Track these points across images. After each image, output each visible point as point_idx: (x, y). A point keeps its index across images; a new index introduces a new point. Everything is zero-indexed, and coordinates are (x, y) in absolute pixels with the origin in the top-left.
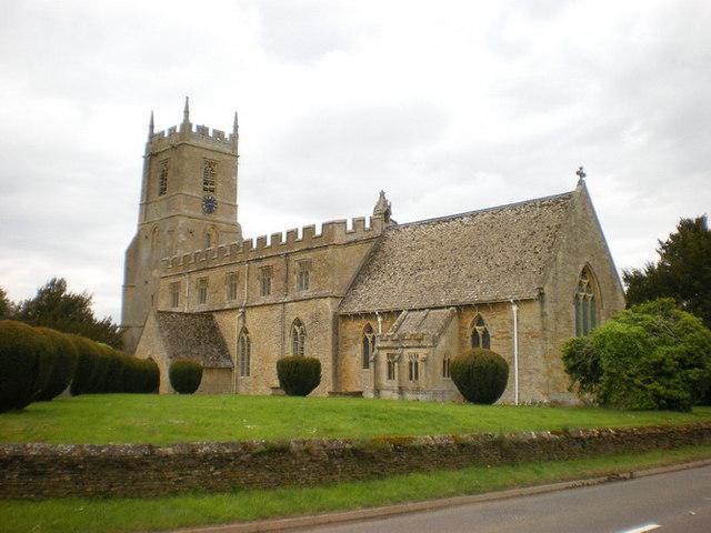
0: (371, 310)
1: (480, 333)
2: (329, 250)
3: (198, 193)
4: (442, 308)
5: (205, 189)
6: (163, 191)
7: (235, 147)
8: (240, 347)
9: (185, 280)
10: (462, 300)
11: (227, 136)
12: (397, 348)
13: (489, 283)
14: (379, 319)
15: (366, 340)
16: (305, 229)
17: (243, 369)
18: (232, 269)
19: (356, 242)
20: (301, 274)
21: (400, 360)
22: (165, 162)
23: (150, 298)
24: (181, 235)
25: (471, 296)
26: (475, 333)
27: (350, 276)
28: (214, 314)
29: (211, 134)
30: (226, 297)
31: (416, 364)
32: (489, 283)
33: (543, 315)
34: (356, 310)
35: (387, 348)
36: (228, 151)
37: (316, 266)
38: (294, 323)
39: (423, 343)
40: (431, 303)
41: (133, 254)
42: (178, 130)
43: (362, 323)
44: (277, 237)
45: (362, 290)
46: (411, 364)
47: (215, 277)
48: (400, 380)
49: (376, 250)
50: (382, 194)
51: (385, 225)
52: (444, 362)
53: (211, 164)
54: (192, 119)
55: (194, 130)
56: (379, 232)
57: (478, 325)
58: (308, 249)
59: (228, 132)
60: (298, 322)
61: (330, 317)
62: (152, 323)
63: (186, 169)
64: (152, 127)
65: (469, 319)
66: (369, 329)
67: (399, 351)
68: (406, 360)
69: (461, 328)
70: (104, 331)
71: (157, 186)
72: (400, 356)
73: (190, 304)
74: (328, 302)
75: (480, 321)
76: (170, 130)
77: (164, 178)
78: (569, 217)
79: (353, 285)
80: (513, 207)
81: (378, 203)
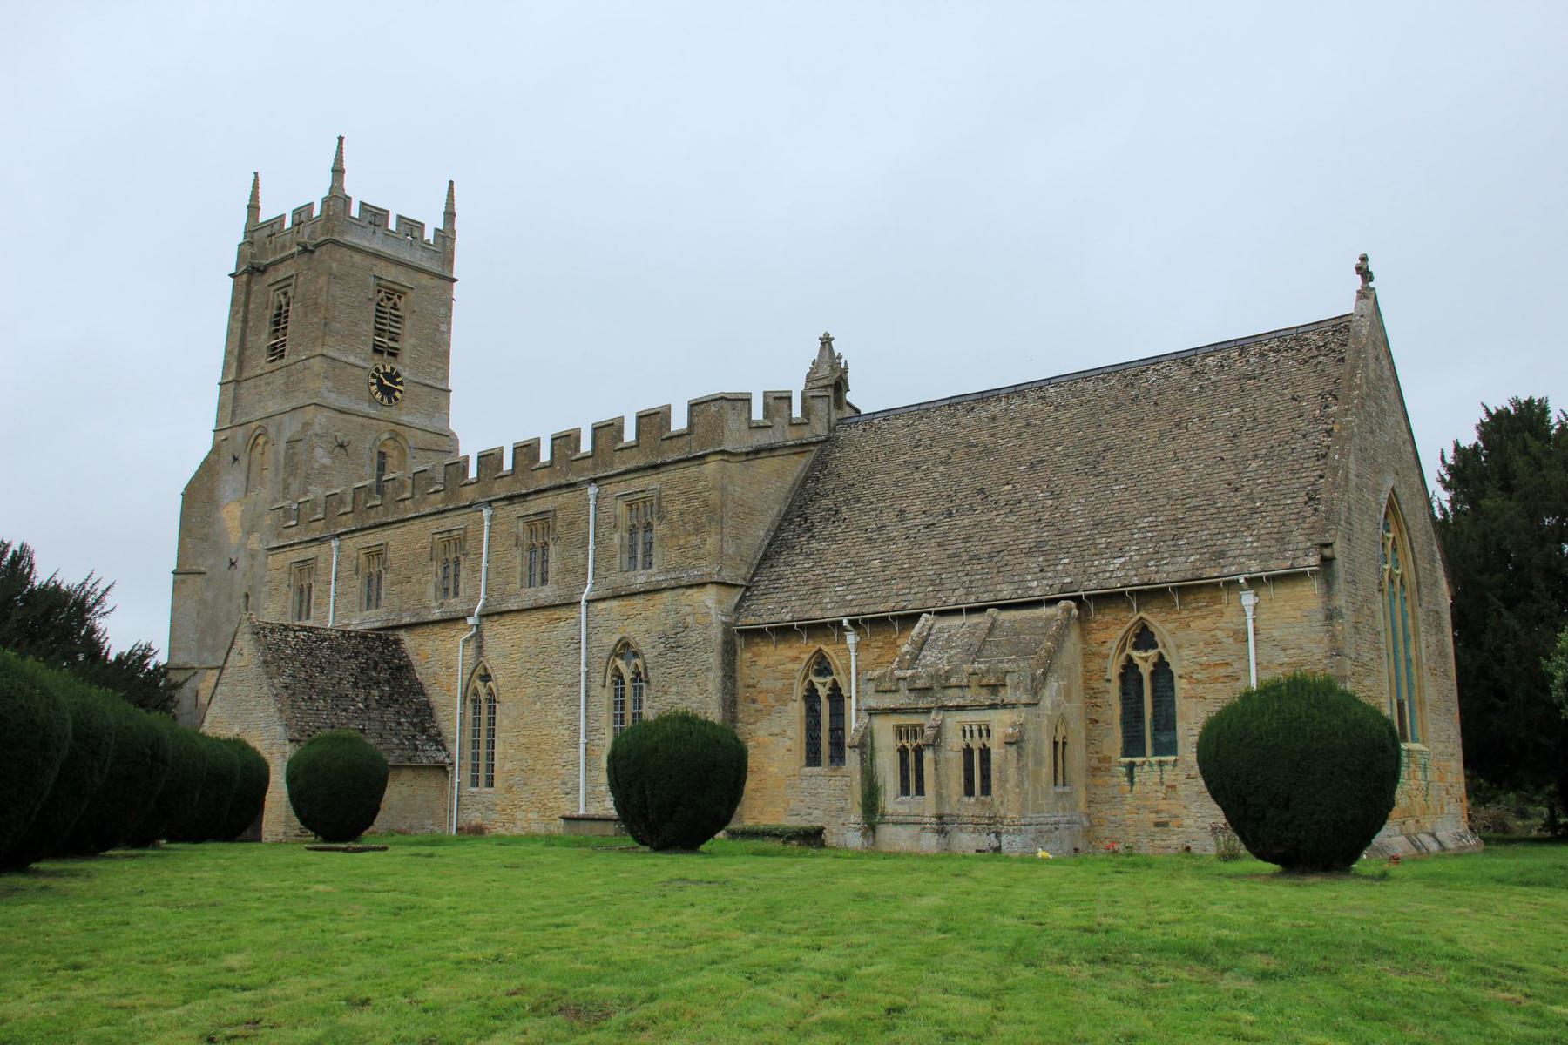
0: (829, 615)
1: (1145, 669)
2: (712, 467)
3: (360, 357)
4: (1037, 604)
5: (378, 350)
6: (276, 352)
7: (448, 259)
8: (470, 714)
9: (332, 556)
10: (1088, 586)
11: (429, 235)
12: (928, 711)
13: (1160, 538)
14: (851, 638)
15: (811, 695)
16: (597, 429)
17: (476, 768)
18: (448, 522)
19: (771, 449)
20: (632, 531)
21: (936, 742)
22: (284, 285)
23: (242, 601)
24: (319, 452)
25: (1114, 573)
26: (1130, 668)
27: (759, 531)
28: (402, 634)
29: (392, 225)
30: (431, 590)
31: (985, 753)
32: (1160, 538)
33: (1331, 615)
34: (786, 617)
35: (894, 711)
36: (438, 270)
37: (675, 507)
38: (616, 654)
39: (1007, 695)
40: (1007, 593)
41: (199, 497)
42: (316, 212)
43: (805, 649)
44: (527, 451)
45: (793, 570)
46: (968, 752)
47: (406, 542)
48: (939, 796)
49: (820, 464)
50: (826, 341)
51: (835, 415)
52: (1056, 744)
53: (392, 293)
54: (351, 187)
55: (355, 212)
56: (821, 431)
57: (1136, 647)
58: (655, 467)
59: (433, 222)
60: (625, 649)
61: (716, 635)
62: (247, 654)
63: (334, 300)
64: (254, 208)
65: (1113, 630)
66: (822, 666)
67: (935, 718)
68: (954, 743)
69: (1088, 656)
70: (133, 676)
71: (262, 339)
72: (939, 730)
73: (339, 611)
74: (709, 596)
75: (1144, 638)
76: (297, 212)
77: (280, 320)
78: (1340, 362)
79: (767, 558)
80: (1185, 358)
81: (815, 365)
